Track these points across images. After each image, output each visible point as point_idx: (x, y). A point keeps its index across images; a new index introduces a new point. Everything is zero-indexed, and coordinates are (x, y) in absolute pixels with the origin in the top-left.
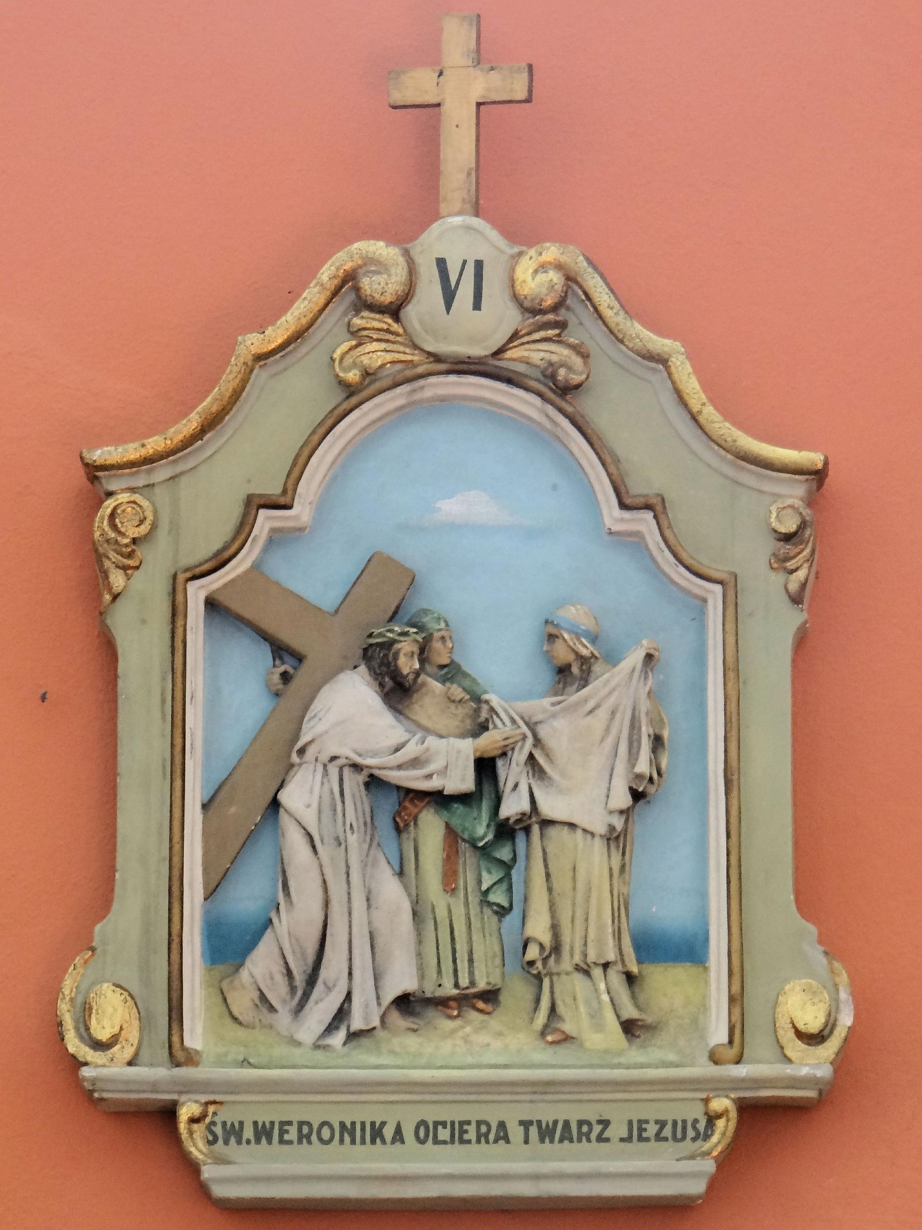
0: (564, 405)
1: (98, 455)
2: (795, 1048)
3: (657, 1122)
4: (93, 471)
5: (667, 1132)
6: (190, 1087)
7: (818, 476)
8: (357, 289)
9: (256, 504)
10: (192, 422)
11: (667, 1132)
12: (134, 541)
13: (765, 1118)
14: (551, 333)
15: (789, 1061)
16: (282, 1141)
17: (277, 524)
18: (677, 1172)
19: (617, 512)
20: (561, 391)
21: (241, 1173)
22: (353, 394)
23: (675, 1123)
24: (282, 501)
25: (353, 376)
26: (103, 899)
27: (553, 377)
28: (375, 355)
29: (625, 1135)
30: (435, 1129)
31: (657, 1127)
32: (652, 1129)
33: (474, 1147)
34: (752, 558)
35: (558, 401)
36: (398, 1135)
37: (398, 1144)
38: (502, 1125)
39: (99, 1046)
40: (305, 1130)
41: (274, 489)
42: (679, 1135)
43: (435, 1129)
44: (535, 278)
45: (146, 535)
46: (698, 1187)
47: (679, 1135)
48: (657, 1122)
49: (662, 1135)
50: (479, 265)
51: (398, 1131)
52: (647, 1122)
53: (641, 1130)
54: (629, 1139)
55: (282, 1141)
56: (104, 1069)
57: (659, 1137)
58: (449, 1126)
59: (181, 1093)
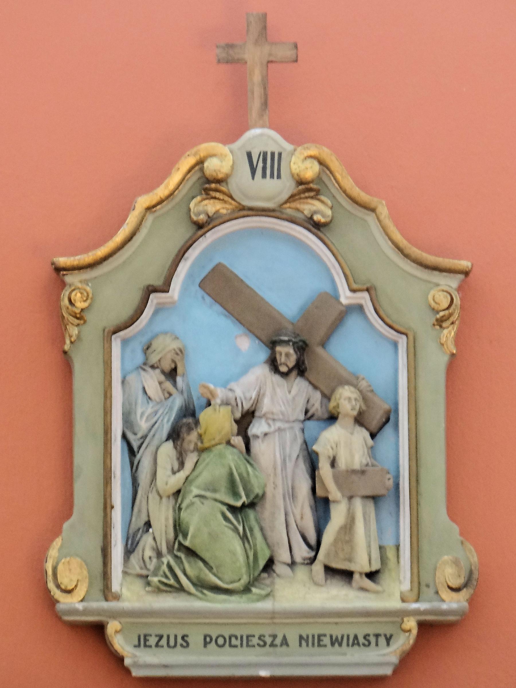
0: (319, 233)
1: (62, 261)
2: (446, 594)
3: (156, 636)
4: (58, 270)
5: (164, 642)
6: (116, 615)
7: (466, 273)
8: (202, 170)
9: (151, 290)
10: (331, 175)
11: (164, 642)
12: (82, 310)
13: (428, 629)
14: (312, 194)
15: (443, 601)
16: (248, 645)
17: (161, 301)
18: (378, 660)
19: (349, 293)
20: (316, 227)
21: (145, 662)
22: (201, 227)
23: (168, 637)
24: (165, 288)
25: (202, 218)
26: (67, 509)
27: (311, 218)
28: (212, 207)
29: (136, 643)
30: (230, 638)
31: (157, 639)
32: (152, 641)
33: (279, 649)
34: (419, 322)
35: (315, 231)
36: (285, 642)
37: (284, 647)
38: (356, 637)
39: (69, 592)
40: (208, 639)
41: (158, 282)
42: (172, 643)
43: (230, 638)
44: (301, 164)
45: (87, 307)
46: (388, 671)
47: (172, 643)
48: (156, 636)
49: (161, 643)
50: (280, 154)
51: (284, 637)
52: (254, 636)
53: (146, 640)
54: (139, 645)
55: (319, 645)
56: (69, 603)
57: (272, 645)
58: (239, 638)
59: (110, 617)
